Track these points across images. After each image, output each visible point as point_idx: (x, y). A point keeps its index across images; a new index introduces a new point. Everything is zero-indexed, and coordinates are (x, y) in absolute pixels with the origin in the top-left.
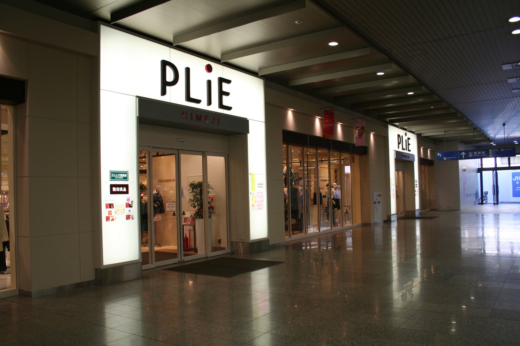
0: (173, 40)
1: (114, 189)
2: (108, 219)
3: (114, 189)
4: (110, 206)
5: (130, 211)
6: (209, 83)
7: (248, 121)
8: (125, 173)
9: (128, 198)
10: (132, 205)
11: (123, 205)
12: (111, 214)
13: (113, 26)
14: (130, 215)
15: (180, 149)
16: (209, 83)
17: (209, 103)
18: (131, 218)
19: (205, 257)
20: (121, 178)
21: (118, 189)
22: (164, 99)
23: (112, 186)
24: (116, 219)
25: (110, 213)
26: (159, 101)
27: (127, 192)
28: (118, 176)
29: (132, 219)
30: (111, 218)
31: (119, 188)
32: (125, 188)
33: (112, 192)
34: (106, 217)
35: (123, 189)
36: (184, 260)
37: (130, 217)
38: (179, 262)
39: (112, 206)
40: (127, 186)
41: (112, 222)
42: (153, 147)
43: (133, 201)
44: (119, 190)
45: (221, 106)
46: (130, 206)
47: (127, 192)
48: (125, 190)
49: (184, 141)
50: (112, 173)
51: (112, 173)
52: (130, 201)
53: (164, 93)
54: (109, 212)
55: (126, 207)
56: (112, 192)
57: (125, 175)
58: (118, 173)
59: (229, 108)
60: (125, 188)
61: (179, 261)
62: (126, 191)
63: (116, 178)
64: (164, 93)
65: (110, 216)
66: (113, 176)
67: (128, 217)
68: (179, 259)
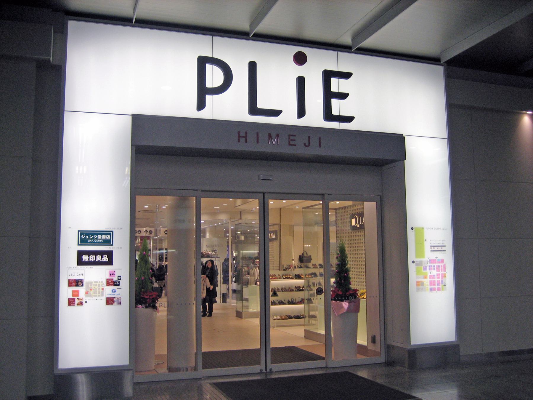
0: (351, 42)
1: (85, 258)
2: (71, 302)
3: (85, 258)
4: (78, 283)
5: (114, 291)
6: (301, 81)
7: (404, 137)
8: (106, 234)
9: (112, 271)
10: (119, 282)
11: (102, 282)
12: (78, 295)
13: (356, 51)
14: (114, 298)
15: (268, 191)
16: (301, 81)
17: (301, 112)
18: (115, 303)
19: (325, 366)
20: (99, 241)
21: (92, 258)
22: (205, 114)
23: (80, 254)
24: (86, 302)
25: (76, 293)
26: (356, 131)
27: (110, 263)
28: (93, 238)
29: (118, 304)
30: (77, 301)
31: (95, 256)
32: (106, 256)
33: (80, 262)
34: (69, 299)
35: (102, 257)
36: (271, 370)
37: (115, 300)
38: (261, 373)
39: (79, 283)
40: (110, 254)
41: (80, 307)
42: (203, 191)
43: (120, 276)
44: (94, 260)
45: (328, 116)
46: (116, 284)
47: (110, 263)
48: (106, 259)
49: (271, 179)
50: (81, 234)
51: (81, 234)
52: (115, 277)
53: (201, 105)
54: (73, 291)
55: (107, 285)
56: (80, 262)
57: (108, 237)
58: (93, 234)
59: (349, 119)
60: (106, 256)
61: (261, 370)
62: (108, 260)
63: (90, 241)
64: (201, 105)
65: (76, 298)
66: (85, 238)
67: (110, 301)
68: (263, 367)
